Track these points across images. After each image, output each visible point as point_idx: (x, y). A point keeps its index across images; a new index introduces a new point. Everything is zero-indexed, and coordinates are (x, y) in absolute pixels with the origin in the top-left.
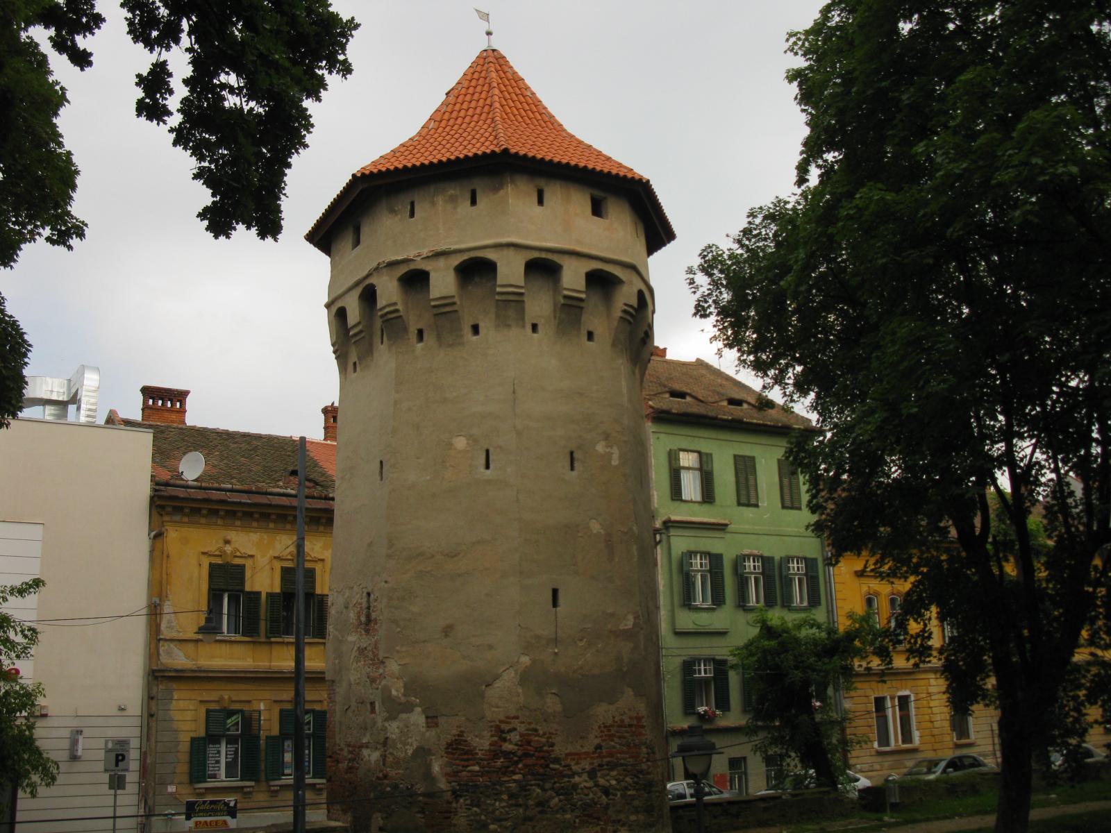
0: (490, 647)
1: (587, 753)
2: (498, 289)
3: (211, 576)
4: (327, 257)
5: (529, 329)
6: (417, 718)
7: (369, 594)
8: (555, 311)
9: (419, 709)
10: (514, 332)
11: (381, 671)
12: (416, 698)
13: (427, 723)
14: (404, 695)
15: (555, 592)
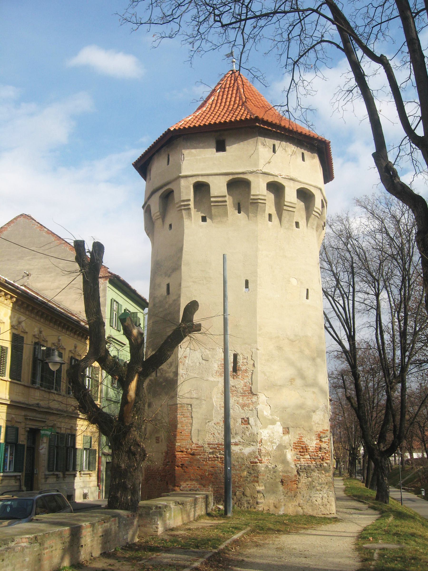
2: (252, 197)
4: (144, 181)
6: (278, 428)
13: (283, 431)
14: (271, 415)
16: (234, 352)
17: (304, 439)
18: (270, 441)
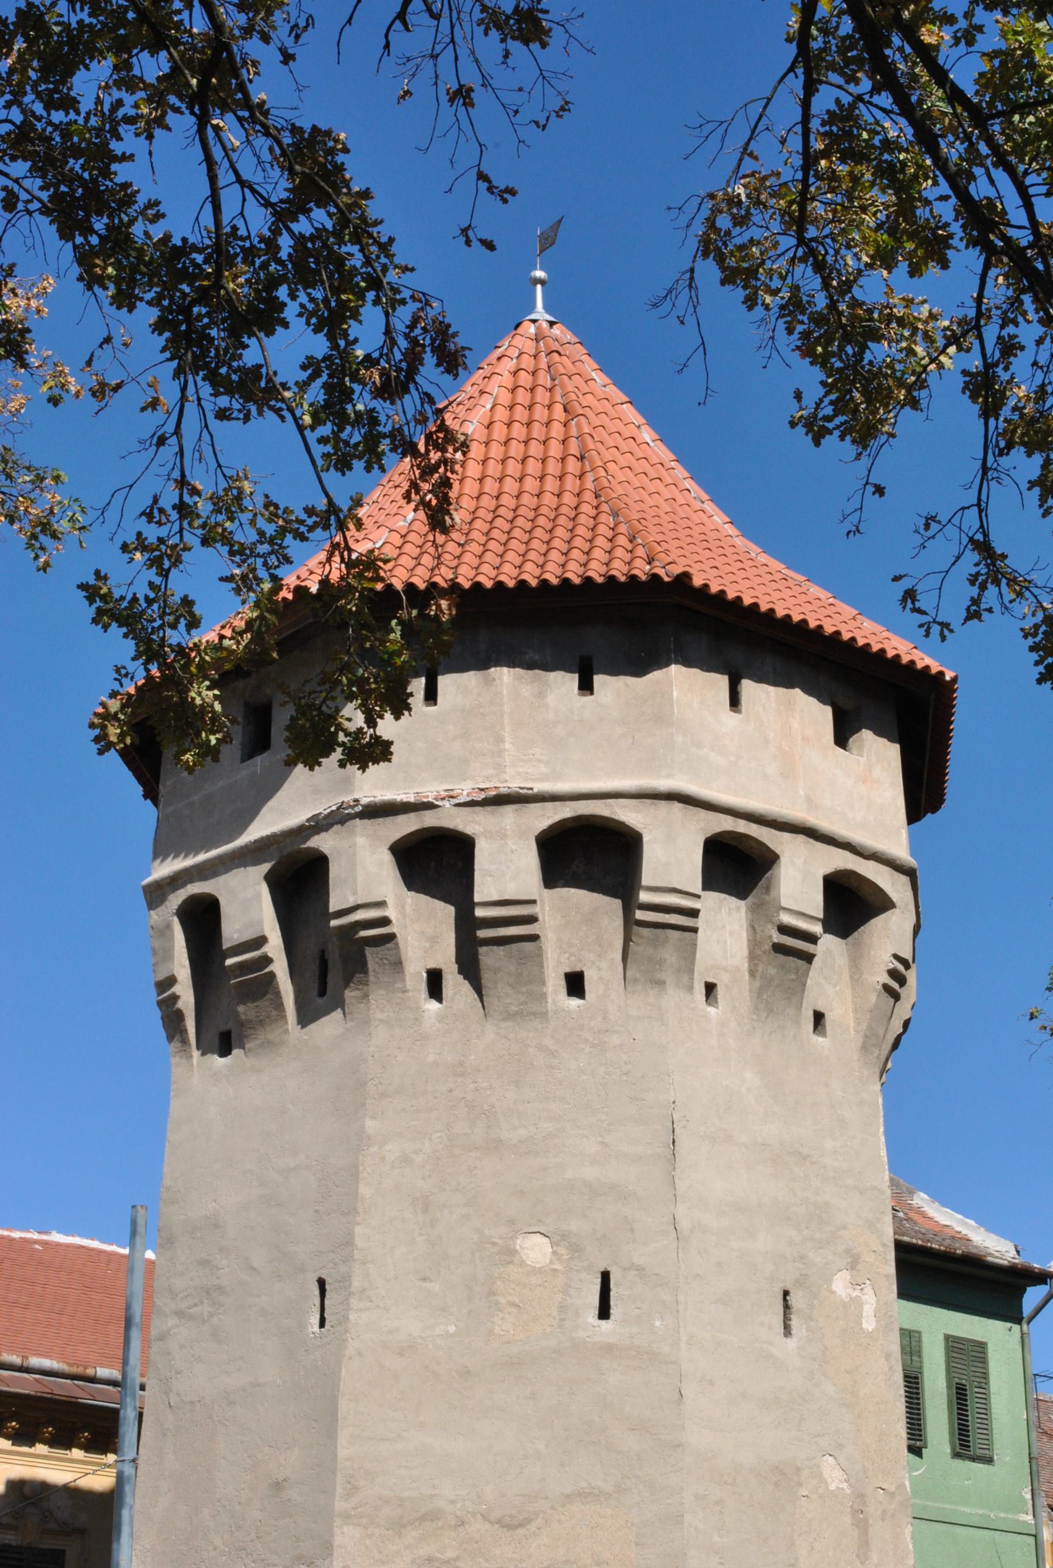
5: (700, 990)
8: (752, 957)
10: (672, 997)
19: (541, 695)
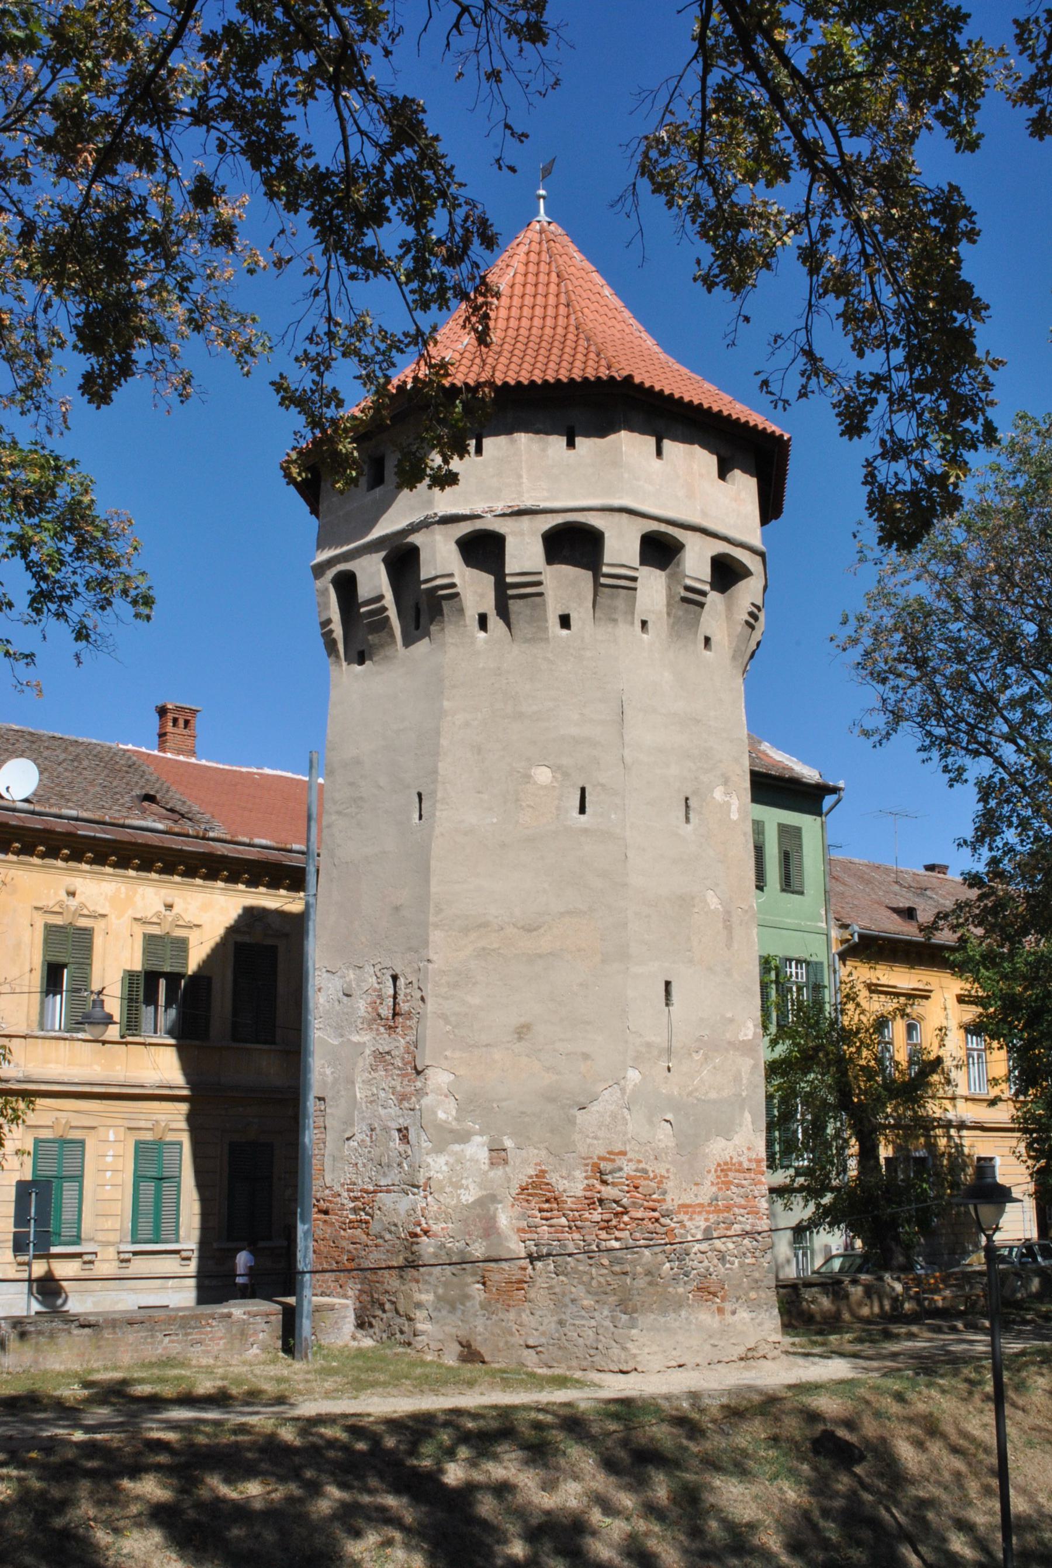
0: (586, 1056)
1: (701, 1205)
3: (46, 941)
7: (395, 978)
8: (669, 605)
9: (478, 1139)
11: (419, 1084)
12: (779, 1108)
13: (491, 1159)
14: (457, 1119)
15: (668, 984)
16: (391, 972)
17: (553, 1178)
18: (451, 1183)
19: (544, 450)
